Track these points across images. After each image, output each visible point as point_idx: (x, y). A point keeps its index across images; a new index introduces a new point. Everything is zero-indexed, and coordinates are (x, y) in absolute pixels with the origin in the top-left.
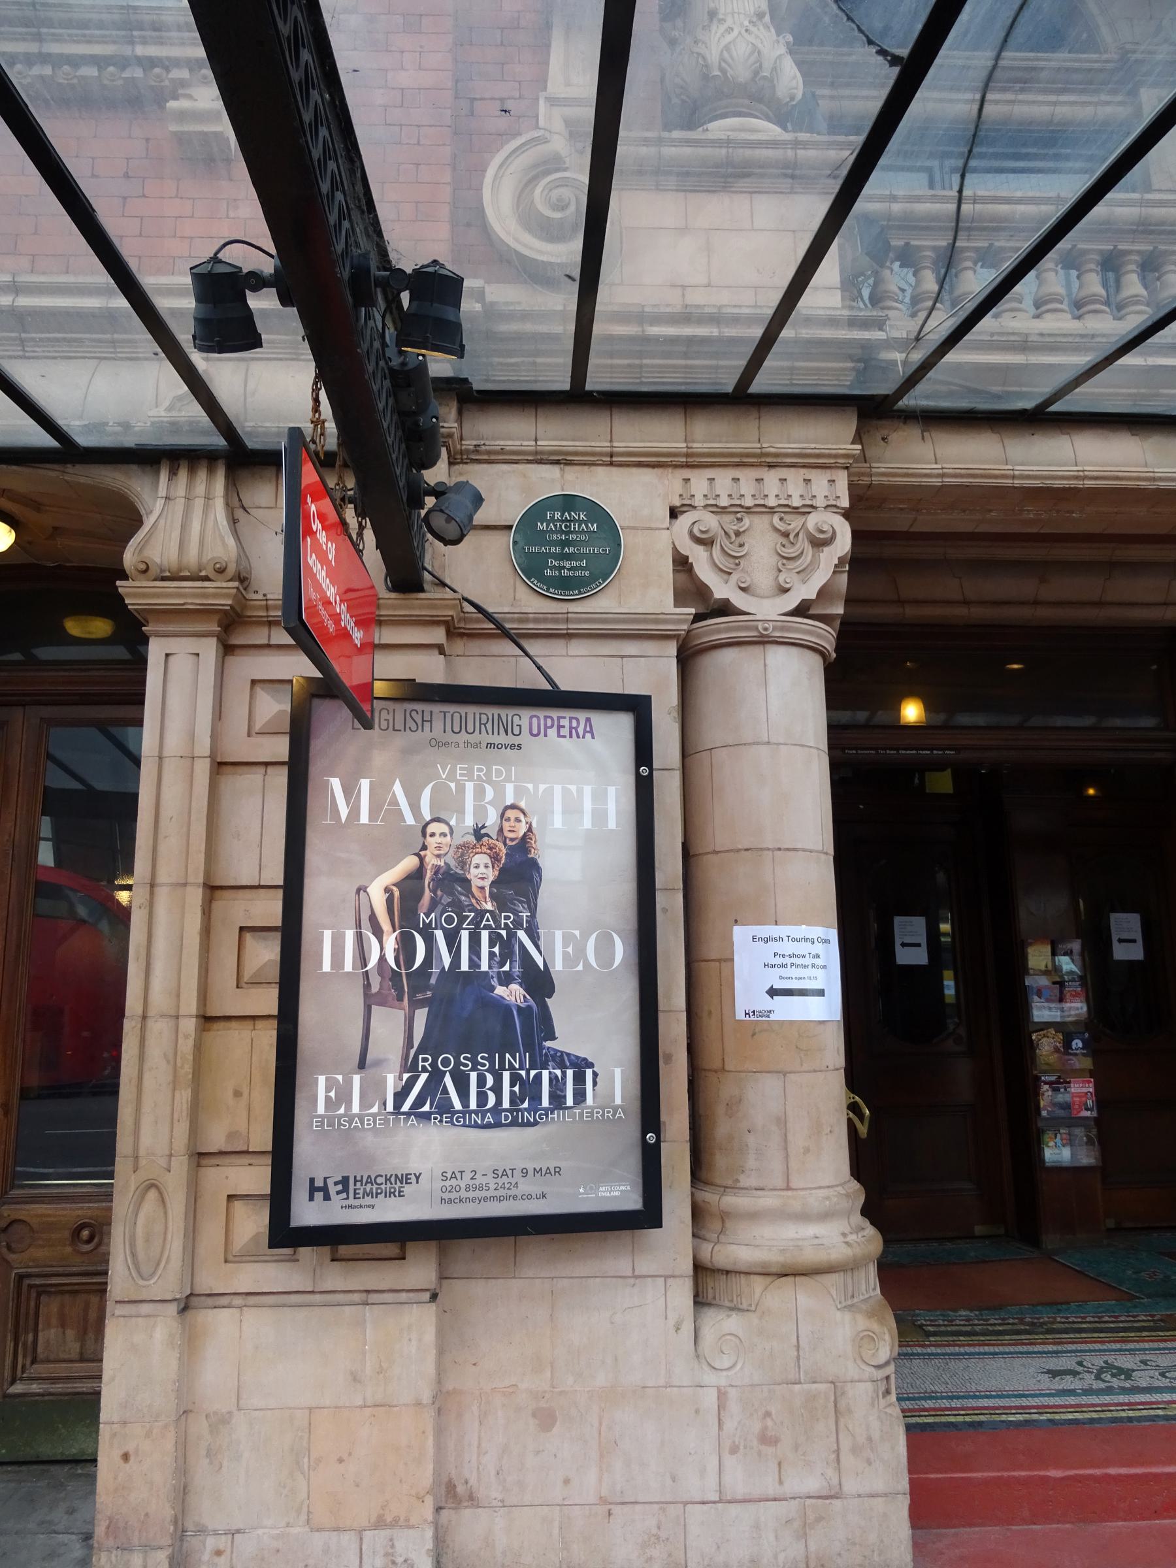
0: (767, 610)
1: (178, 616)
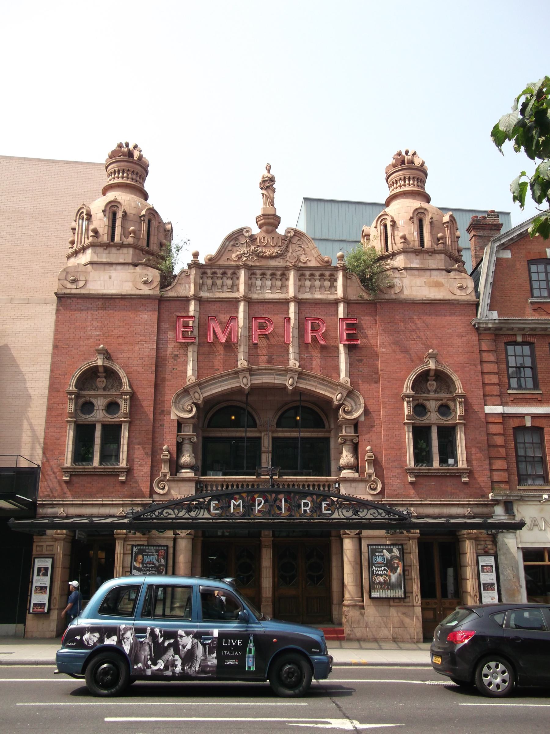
1: (119, 539)
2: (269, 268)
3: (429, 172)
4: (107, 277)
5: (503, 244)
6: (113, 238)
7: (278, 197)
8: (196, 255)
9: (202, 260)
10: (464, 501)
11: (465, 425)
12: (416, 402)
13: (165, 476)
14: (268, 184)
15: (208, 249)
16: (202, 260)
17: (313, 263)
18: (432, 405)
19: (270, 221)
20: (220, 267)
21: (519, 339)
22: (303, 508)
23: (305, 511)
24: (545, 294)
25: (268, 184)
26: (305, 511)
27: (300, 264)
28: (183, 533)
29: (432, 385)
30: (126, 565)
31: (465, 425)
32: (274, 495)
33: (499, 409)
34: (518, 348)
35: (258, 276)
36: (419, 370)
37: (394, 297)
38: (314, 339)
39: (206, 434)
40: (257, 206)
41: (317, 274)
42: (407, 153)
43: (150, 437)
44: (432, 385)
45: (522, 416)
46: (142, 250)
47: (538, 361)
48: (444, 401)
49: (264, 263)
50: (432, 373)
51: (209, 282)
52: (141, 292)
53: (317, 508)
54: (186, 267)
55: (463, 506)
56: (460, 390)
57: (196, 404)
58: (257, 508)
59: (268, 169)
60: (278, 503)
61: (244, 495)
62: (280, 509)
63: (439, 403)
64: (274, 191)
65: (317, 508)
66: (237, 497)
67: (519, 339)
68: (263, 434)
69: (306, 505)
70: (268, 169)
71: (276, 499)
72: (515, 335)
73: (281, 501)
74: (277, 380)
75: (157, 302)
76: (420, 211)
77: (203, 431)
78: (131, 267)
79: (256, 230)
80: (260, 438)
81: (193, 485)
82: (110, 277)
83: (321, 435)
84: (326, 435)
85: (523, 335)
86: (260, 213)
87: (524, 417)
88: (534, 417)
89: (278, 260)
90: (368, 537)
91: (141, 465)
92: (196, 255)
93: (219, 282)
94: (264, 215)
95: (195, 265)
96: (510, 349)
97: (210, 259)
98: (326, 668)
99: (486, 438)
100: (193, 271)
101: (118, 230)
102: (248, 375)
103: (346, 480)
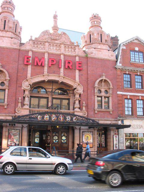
0: (25, 126)
2: (55, 43)
3: (102, 19)
4: (2, 41)
5: (124, 44)
6: (4, 29)
7: (58, 21)
8: (31, 37)
9: (33, 39)
10: (111, 119)
11: (112, 97)
12: (98, 89)
13: (19, 107)
14: (55, 17)
15: (36, 35)
16: (33, 39)
17: (69, 44)
18: (103, 90)
19: (55, 28)
20: (39, 41)
21: (127, 73)
22: (67, 119)
23: (68, 120)
24: (142, 62)
25: (55, 17)
26: (68, 120)
27: (65, 43)
28: (25, 125)
29: (103, 84)
30: (6, 135)
31: (112, 97)
32: (58, 115)
33: (121, 93)
34: (126, 75)
35: (51, 46)
36: (100, 79)
37: (93, 56)
38: (68, 66)
39: (31, 95)
40: (52, 24)
41: (70, 47)
42: (96, 14)
43: (15, 94)
44: (103, 84)
45: (139, 96)
46: (14, 33)
47: (132, 80)
48: (107, 89)
49: (53, 41)
50: (103, 80)
51: (36, 46)
52: (13, 47)
53: (72, 119)
54: (28, 41)
55: (110, 121)
56: (111, 87)
57: (30, 85)
58: (53, 119)
59: (56, 12)
60: (60, 117)
61: (49, 114)
62: (60, 119)
63: (105, 90)
64: (57, 19)
65: (72, 119)
66: (47, 115)
67: (127, 73)
68: (49, 96)
69: (69, 118)
70: (56, 12)
71: (59, 116)
72: (126, 71)
73: (61, 117)
74: (57, 79)
75: (18, 50)
76: (101, 31)
77: (30, 94)
78: (107, 51)
79: (52, 31)
80: (48, 97)
81: (28, 111)
82: (3, 41)
83: (67, 98)
84: (69, 98)
85: (140, 73)
86: (53, 26)
87: (139, 96)
88: (130, 96)
89: (57, 41)
90: (83, 129)
91: (12, 103)
92: (31, 37)
93: (39, 46)
94: (54, 26)
95: (31, 40)
96: (124, 75)
97: (36, 39)
98: (103, 162)
99: (117, 101)
100: (31, 42)
101: (6, 26)
102: (47, 77)
103: (76, 112)
